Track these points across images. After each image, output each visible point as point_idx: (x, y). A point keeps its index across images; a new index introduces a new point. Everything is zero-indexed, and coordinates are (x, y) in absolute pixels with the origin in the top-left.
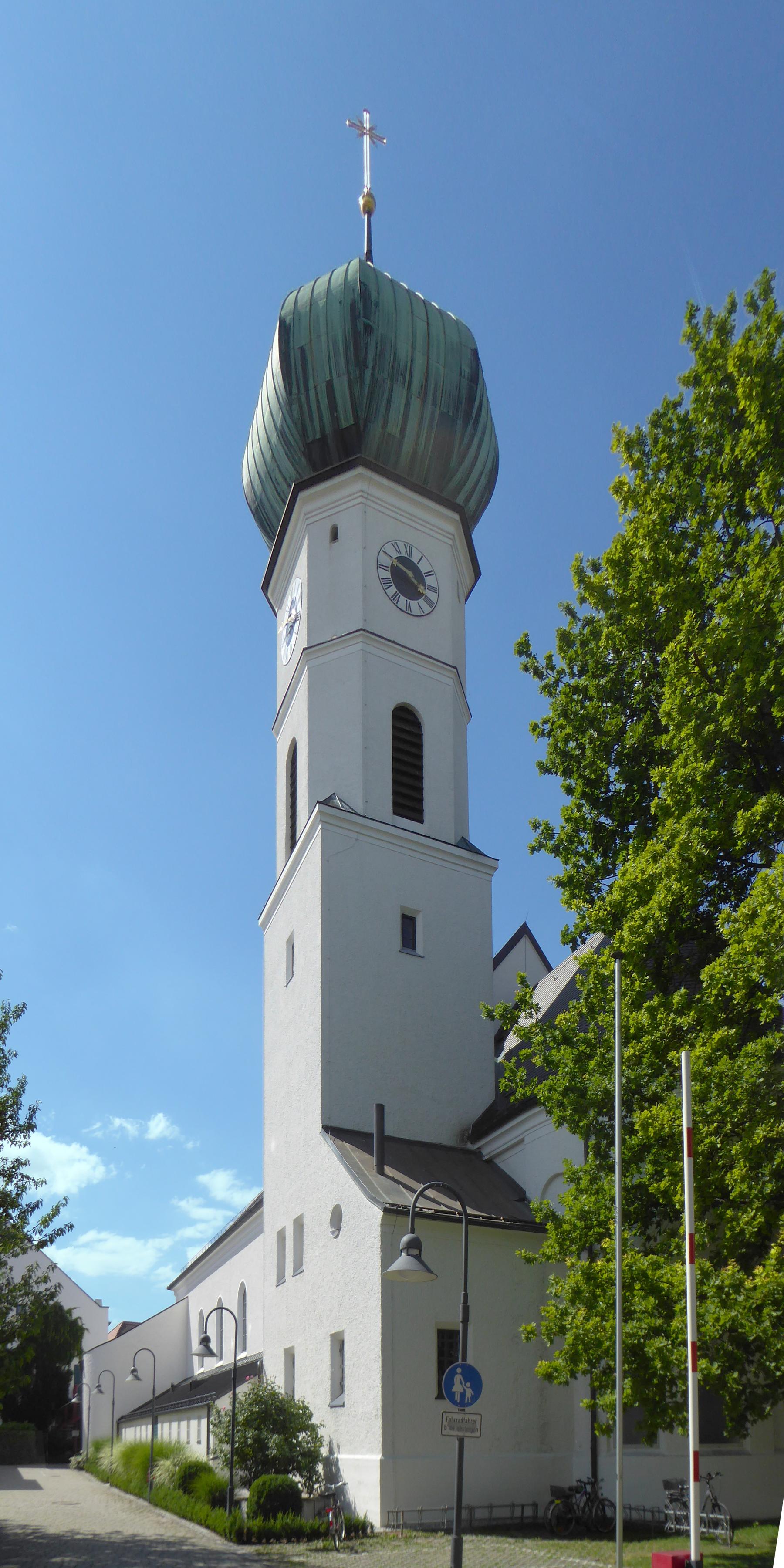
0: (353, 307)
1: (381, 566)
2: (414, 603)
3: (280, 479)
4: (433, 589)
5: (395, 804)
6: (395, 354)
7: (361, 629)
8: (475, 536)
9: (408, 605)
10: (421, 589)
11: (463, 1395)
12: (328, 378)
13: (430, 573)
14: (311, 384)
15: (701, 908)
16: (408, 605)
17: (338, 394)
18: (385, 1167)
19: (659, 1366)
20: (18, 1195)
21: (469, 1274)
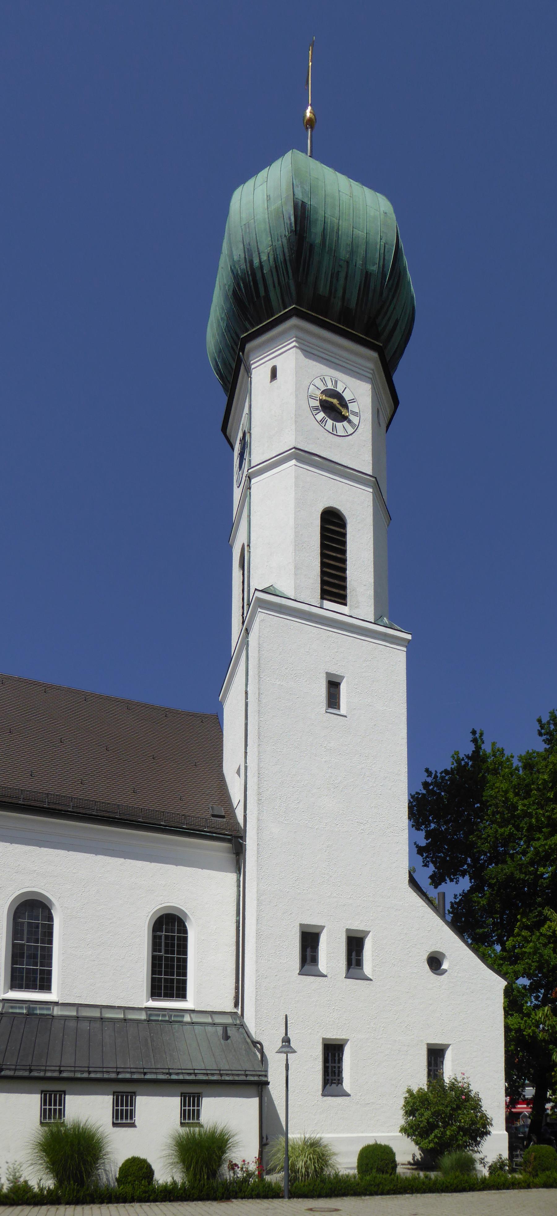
1: (311, 397)
2: (339, 425)
4: (356, 414)
7: (294, 448)
8: (395, 378)
9: (334, 428)
10: (344, 412)
13: (353, 401)
16: (334, 428)
19: (548, 1106)
21: (284, 1107)
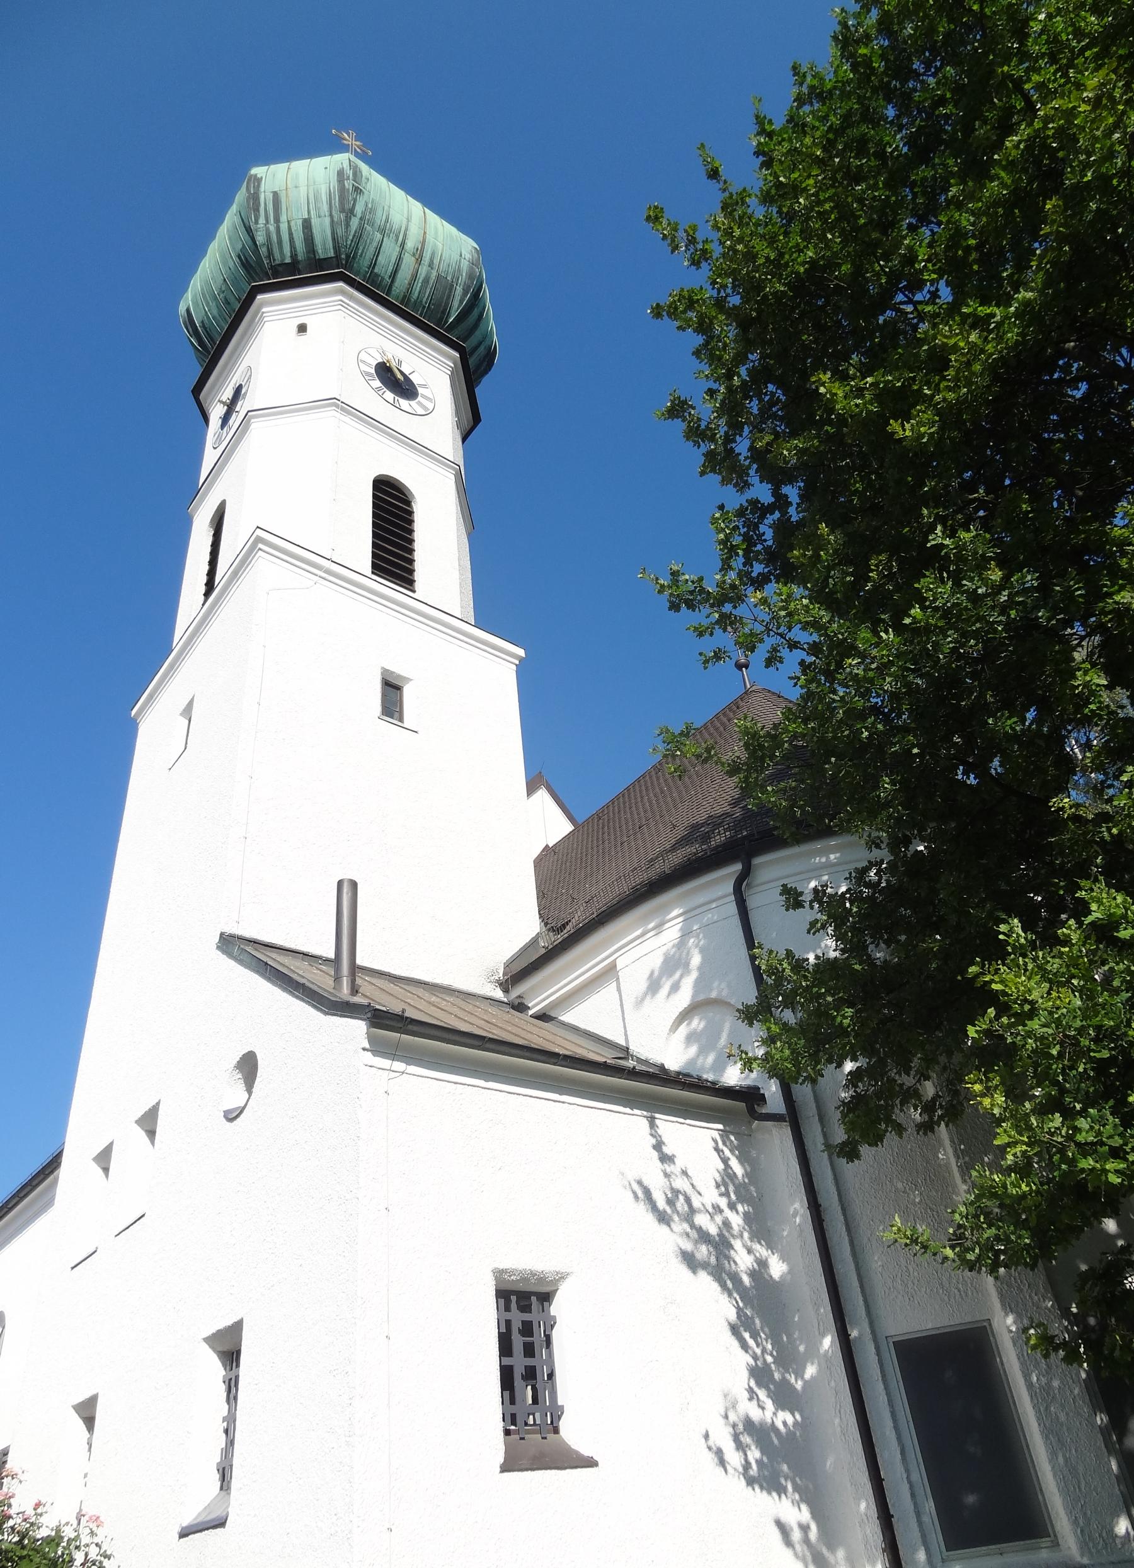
14: (283, 218)
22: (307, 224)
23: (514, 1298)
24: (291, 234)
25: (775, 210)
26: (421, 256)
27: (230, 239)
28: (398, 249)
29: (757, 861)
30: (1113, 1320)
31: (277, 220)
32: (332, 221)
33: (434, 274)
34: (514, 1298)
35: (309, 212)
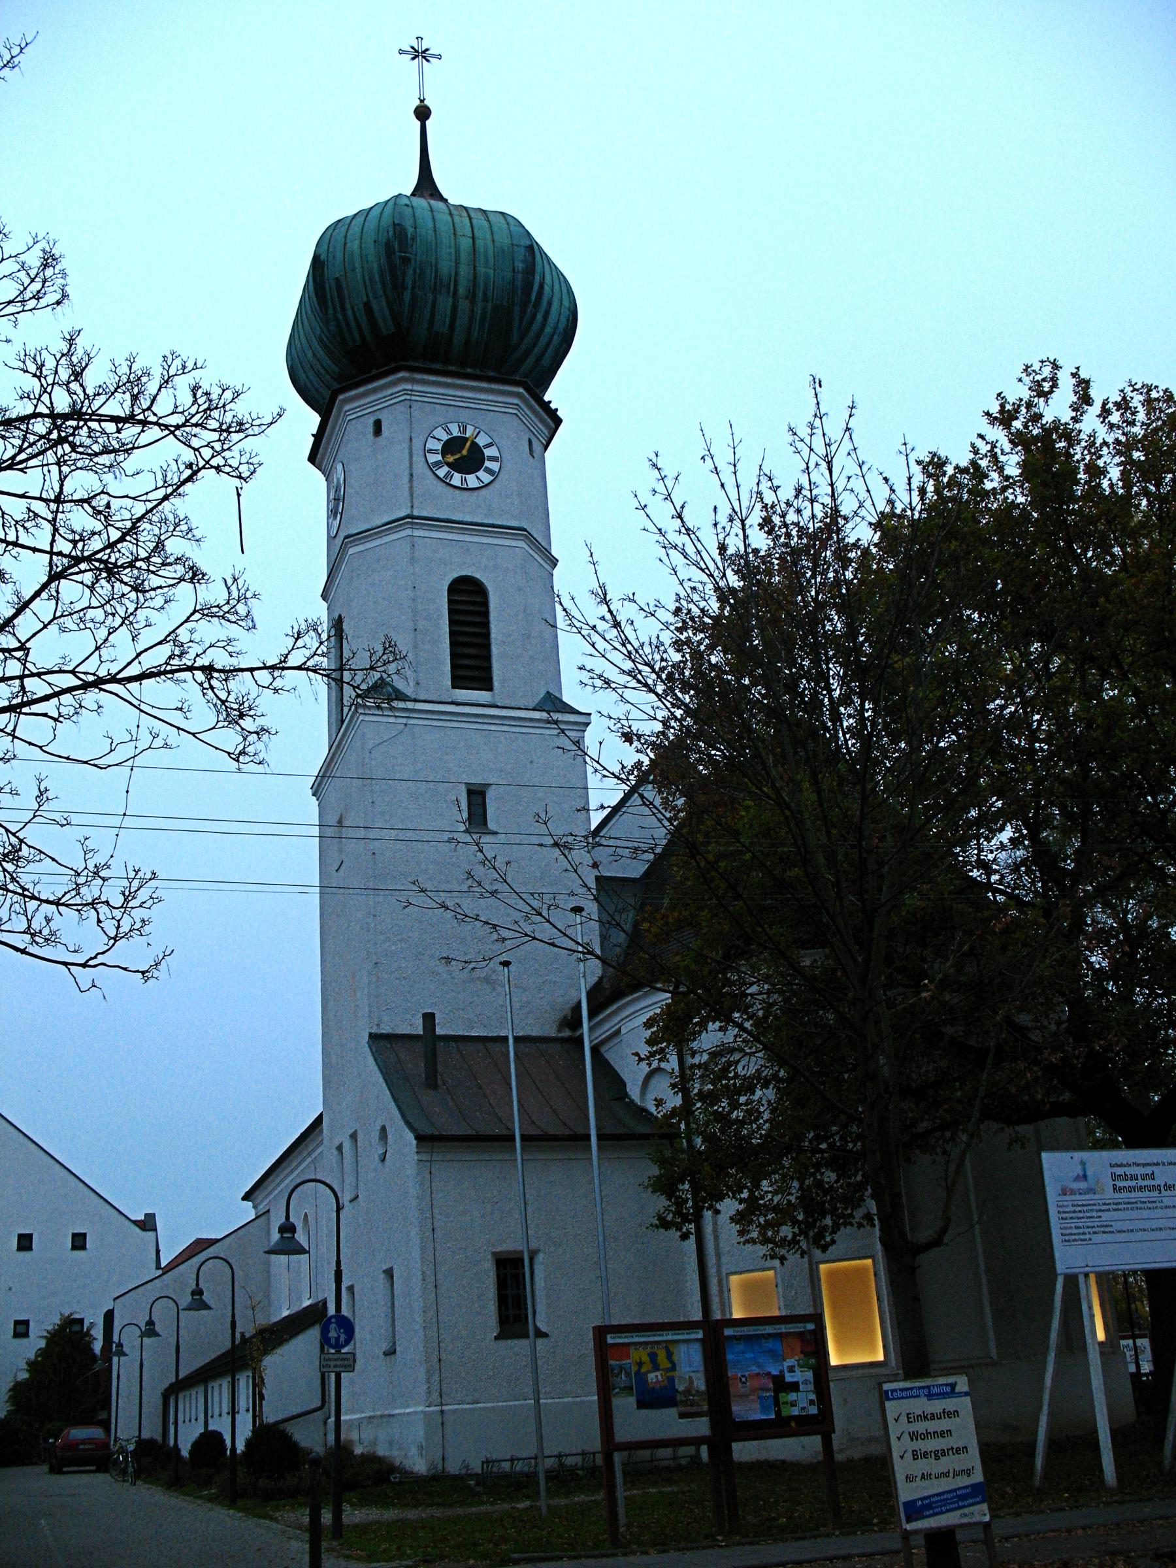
0: (388, 244)
3: (322, 371)
5: (453, 678)
6: (436, 272)
11: (337, 1339)
12: (365, 300)
14: (348, 306)
15: (804, 681)
17: (377, 313)
18: (665, 997)
20: (1076, 420)
22: (368, 306)
23: (811, 1326)
24: (356, 320)
25: (394, 1547)
26: (474, 295)
27: (320, 340)
28: (451, 300)
29: (228, 1345)
30: (812, 1134)
31: (343, 308)
32: (388, 301)
33: (490, 305)
34: (811, 1326)
35: (367, 296)
